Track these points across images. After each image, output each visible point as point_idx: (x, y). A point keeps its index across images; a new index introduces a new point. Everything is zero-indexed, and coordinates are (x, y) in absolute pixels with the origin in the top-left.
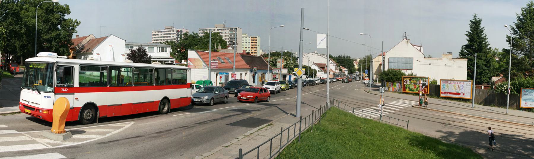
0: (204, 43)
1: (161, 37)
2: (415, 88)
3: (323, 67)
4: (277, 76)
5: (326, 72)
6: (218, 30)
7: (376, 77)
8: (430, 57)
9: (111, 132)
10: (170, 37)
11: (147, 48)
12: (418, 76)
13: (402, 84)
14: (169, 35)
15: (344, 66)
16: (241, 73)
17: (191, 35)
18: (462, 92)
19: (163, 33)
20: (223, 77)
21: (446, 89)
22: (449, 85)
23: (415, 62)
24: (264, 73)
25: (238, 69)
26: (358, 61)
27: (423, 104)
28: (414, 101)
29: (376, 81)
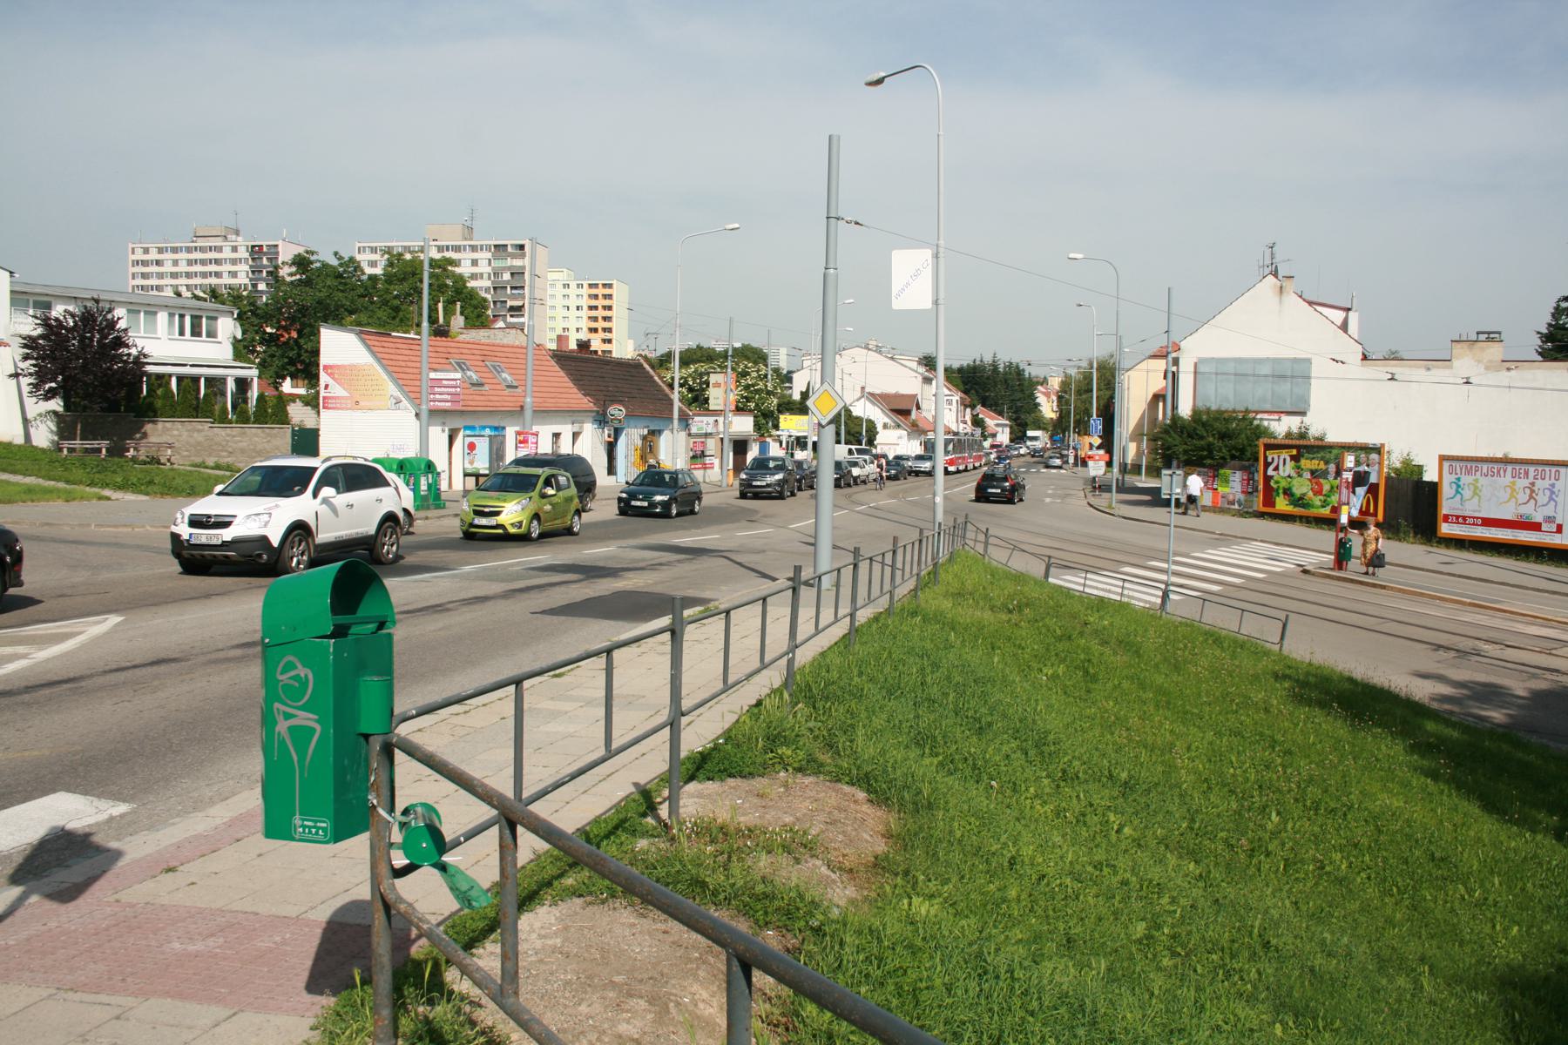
0: (385, 303)
1: (174, 275)
2: (1318, 492)
3: (902, 410)
4: (712, 446)
5: (916, 430)
7: (1139, 453)
8: (1394, 357)
9: (24, 656)
10: (218, 275)
11: (120, 312)
12: (1331, 438)
13: (1259, 477)
14: (213, 268)
15: (994, 406)
16: (556, 428)
17: (325, 265)
18: (1550, 520)
19: (183, 256)
20: (483, 446)
21: (1459, 503)
22: (1483, 481)
23: (1319, 368)
24: (652, 433)
25: (543, 414)
26: (1055, 383)
27: (1355, 565)
28: (1315, 550)
29: (1136, 469)
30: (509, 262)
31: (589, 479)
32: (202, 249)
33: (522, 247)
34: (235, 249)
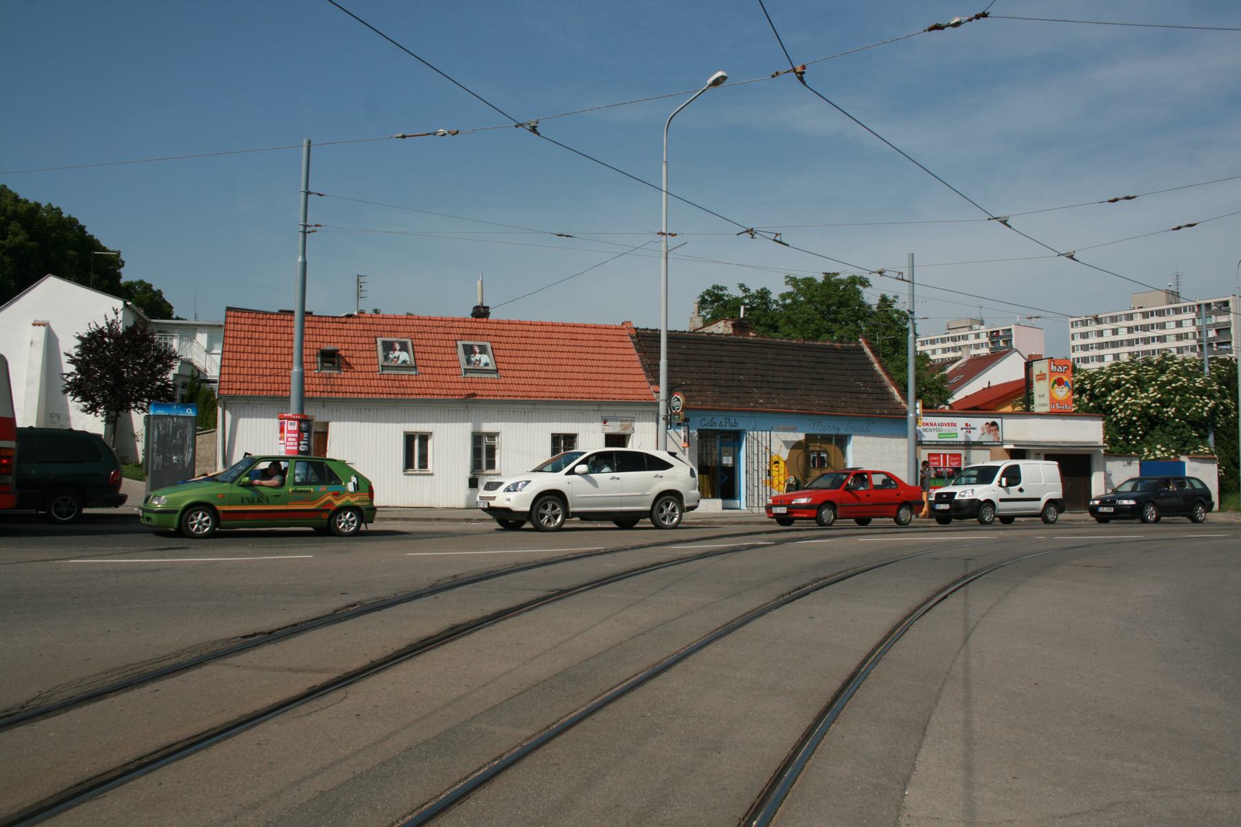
6: (1145, 315)
19: (939, 346)
30: (1214, 319)
31: (10, 416)
32: (954, 339)
33: (1226, 303)
34: (977, 336)
